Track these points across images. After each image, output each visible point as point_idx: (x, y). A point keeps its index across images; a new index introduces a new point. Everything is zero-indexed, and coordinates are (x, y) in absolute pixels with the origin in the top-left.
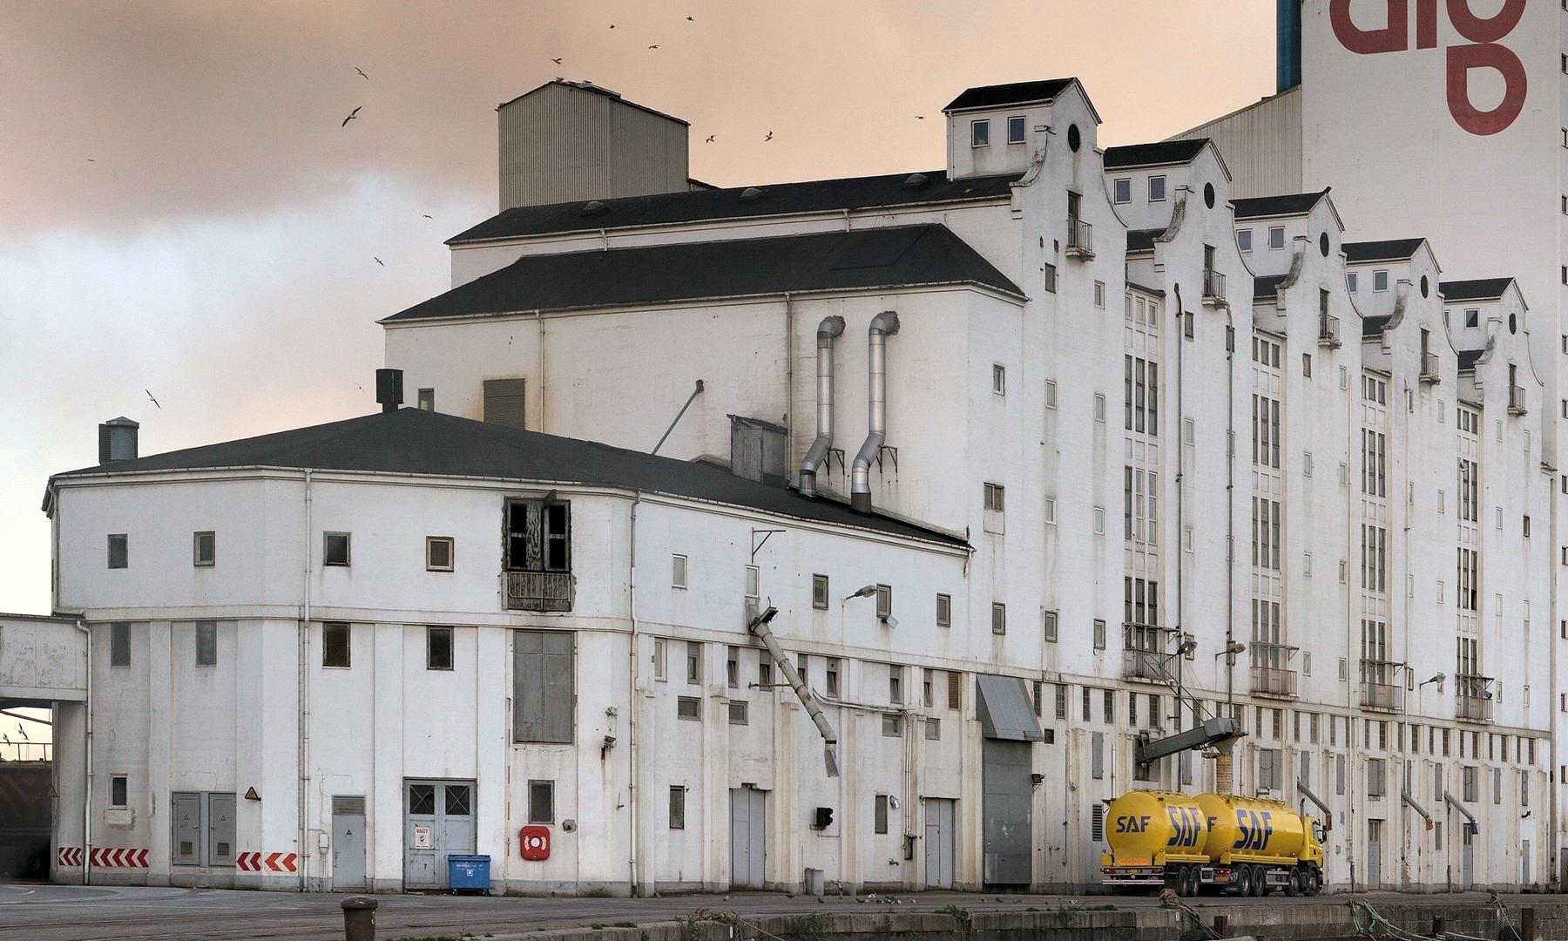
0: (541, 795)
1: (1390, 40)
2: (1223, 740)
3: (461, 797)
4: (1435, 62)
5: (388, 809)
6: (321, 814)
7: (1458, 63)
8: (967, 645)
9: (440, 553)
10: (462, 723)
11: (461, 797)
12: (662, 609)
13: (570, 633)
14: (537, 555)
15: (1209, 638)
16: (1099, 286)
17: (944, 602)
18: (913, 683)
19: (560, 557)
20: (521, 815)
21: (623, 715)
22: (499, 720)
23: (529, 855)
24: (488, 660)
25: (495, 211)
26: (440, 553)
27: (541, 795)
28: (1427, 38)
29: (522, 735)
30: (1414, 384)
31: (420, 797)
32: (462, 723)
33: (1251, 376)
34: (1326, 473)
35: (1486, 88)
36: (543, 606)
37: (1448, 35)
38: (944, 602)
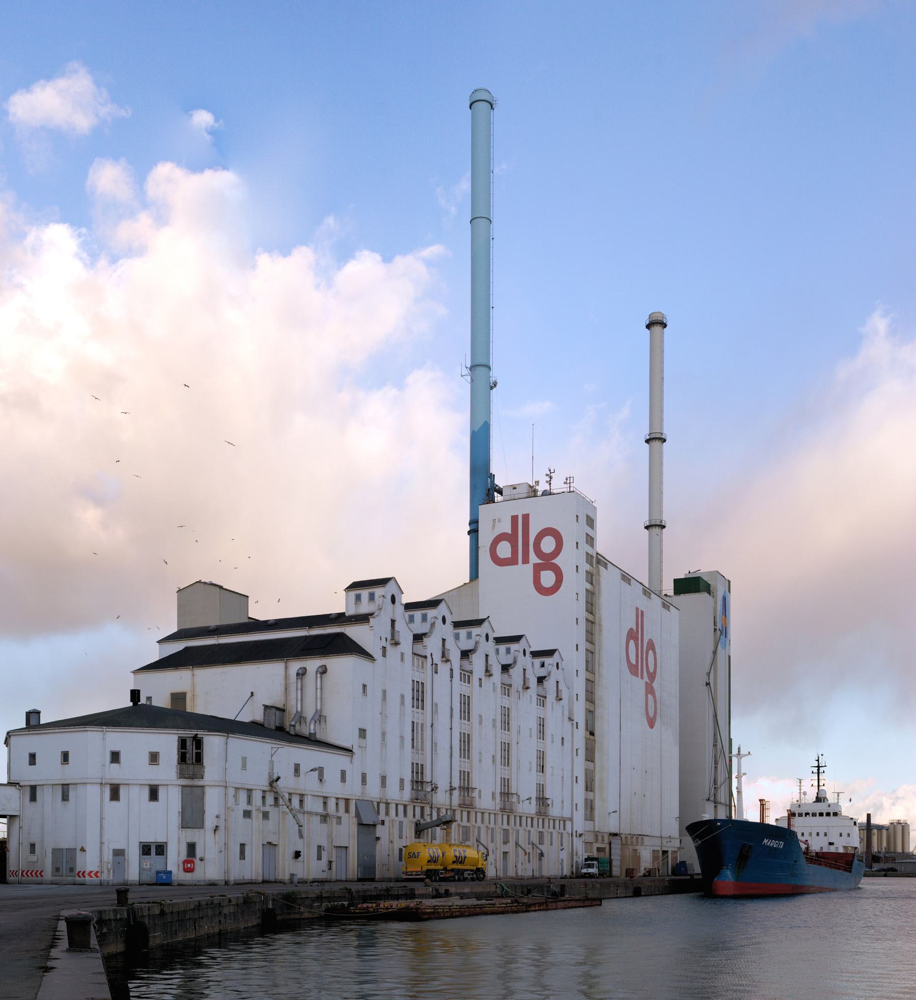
0: (191, 847)
1: (512, 561)
2: (448, 823)
3: (161, 849)
4: (528, 569)
5: (134, 854)
6: (108, 856)
7: (538, 569)
8: (352, 789)
9: (154, 758)
10: (162, 821)
11: (161, 849)
12: (237, 777)
13: (203, 787)
14: (191, 757)
15: (443, 783)
16: (402, 654)
17: (343, 773)
18: (332, 804)
19: (199, 759)
20: (184, 856)
21: (222, 817)
22: (175, 819)
23: (187, 870)
24: (172, 798)
25: (176, 630)
26: (154, 758)
27: (191, 847)
28: (526, 560)
29: (185, 825)
30: (520, 689)
31: (146, 849)
32: (162, 821)
33: (459, 687)
34: (487, 760)
35: (548, 578)
36: (193, 777)
37: (534, 559)
38: (343, 773)
